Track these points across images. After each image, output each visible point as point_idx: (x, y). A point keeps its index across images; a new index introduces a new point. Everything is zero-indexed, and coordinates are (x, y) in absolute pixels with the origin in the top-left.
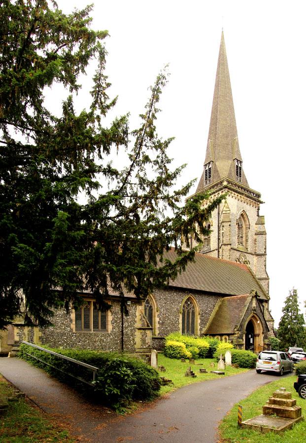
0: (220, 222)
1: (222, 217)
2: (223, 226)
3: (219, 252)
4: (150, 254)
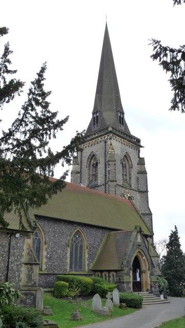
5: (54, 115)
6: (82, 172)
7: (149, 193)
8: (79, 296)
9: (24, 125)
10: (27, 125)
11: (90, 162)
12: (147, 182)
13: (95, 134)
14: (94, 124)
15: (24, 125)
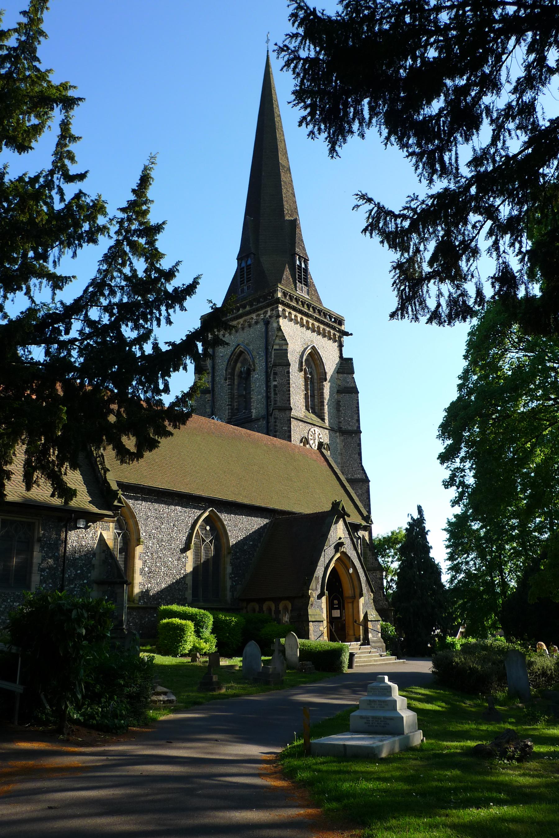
0: (270, 365)
1: (273, 356)
2: (275, 374)
3: (268, 422)
4: (170, 701)
5: (170, 275)
6: (216, 389)
7: (362, 435)
8: (306, 285)
9: (107, 292)
10: (113, 293)
11: (234, 369)
12: (358, 410)
13: (244, 307)
14: (242, 282)
15: (107, 292)
